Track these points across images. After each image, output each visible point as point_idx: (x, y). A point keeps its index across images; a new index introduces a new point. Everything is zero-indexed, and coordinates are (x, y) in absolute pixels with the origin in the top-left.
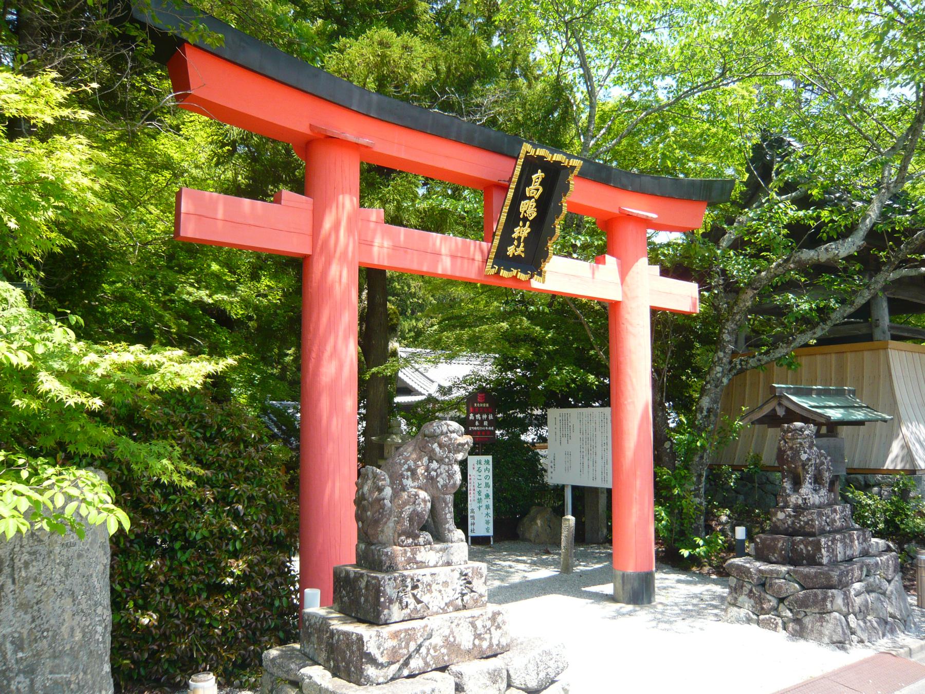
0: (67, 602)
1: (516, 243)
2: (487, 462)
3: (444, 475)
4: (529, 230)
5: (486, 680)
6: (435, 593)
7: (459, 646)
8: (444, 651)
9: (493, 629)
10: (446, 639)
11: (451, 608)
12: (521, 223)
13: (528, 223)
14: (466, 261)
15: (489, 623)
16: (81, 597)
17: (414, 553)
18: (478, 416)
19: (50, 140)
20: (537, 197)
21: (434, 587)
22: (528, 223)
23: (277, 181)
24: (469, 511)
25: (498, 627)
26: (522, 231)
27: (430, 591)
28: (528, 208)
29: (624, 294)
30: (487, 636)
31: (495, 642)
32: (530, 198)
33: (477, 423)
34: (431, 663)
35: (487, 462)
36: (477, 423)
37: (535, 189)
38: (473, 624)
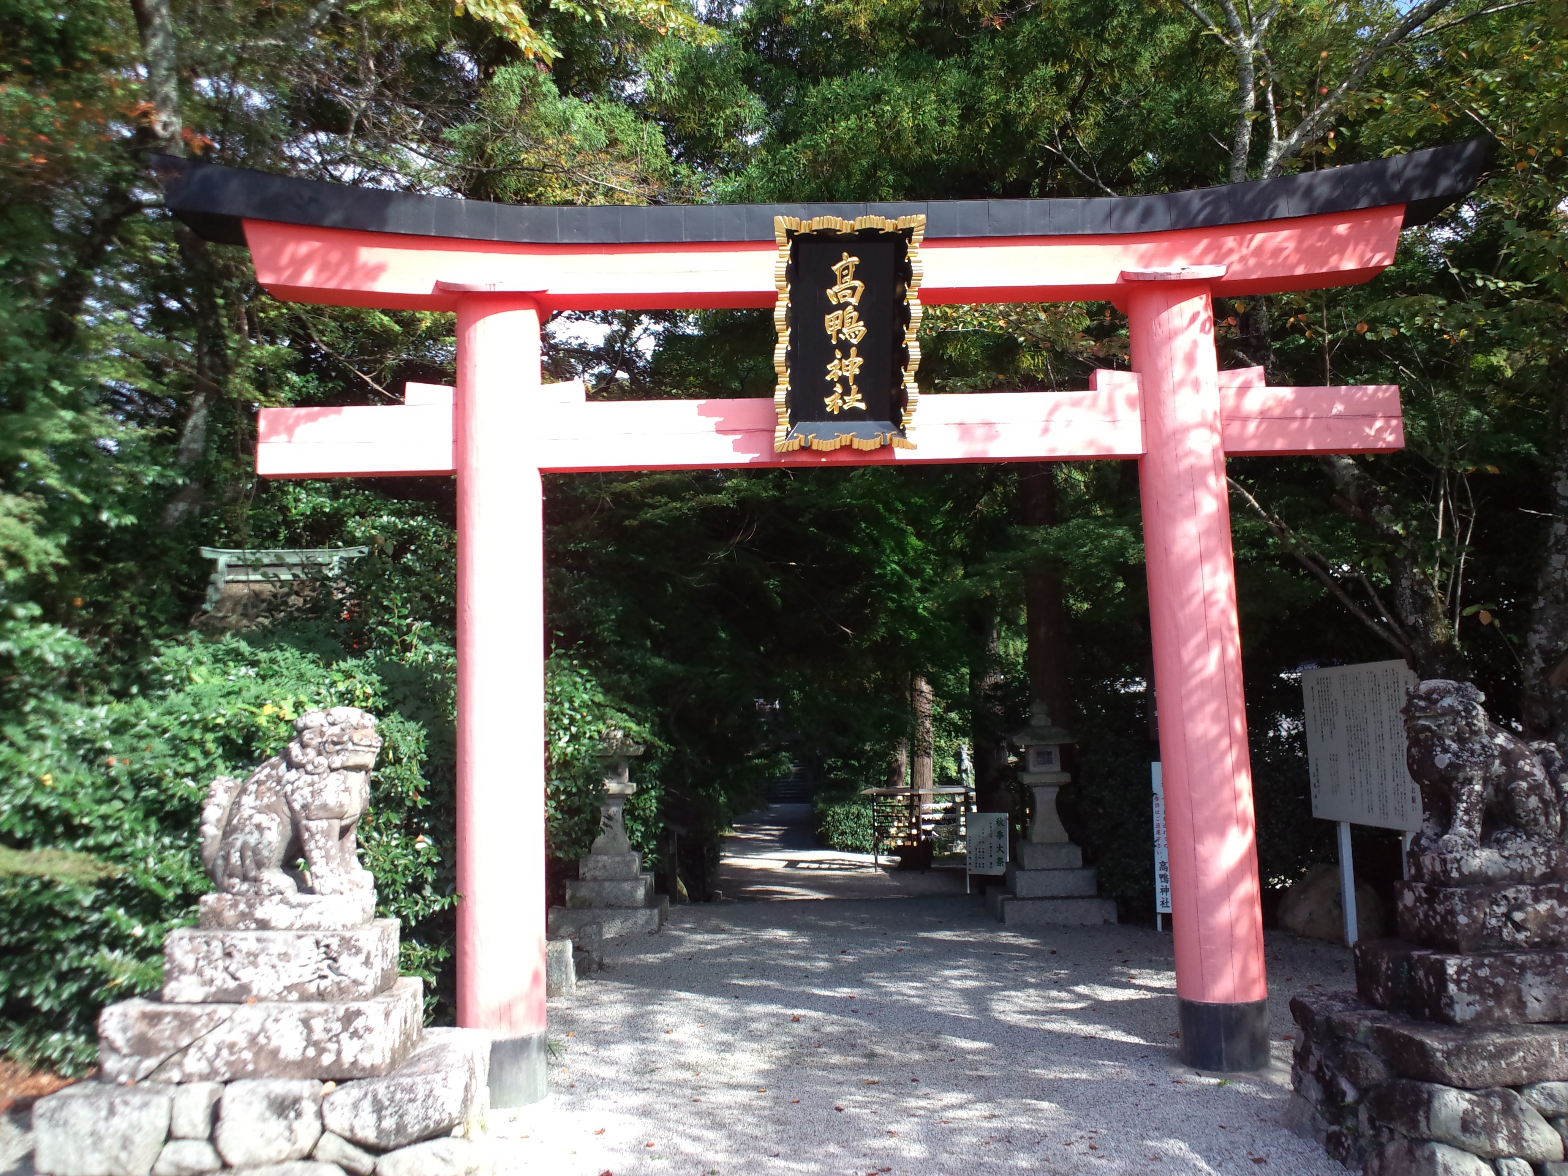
1: (838, 389)
3: (306, 792)
4: (859, 361)
5: (260, 1106)
6: (264, 969)
7: (275, 1052)
8: (247, 1055)
9: (345, 1037)
10: (253, 1040)
11: (295, 995)
12: (838, 354)
13: (853, 351)
15: (337, 1027)
17: (251, 906)
19: (1106, 340)
20: (854, 301)
21: (262, 959)
22: (853, 351)
24: (1157, 866)
25: (355, 1034)
26: (846, 367)
27: (255, 964)
28: (847, 325)
30: (333, 1046)
32: (843, 306)
34: (223, 1070)
37: (846, 290)
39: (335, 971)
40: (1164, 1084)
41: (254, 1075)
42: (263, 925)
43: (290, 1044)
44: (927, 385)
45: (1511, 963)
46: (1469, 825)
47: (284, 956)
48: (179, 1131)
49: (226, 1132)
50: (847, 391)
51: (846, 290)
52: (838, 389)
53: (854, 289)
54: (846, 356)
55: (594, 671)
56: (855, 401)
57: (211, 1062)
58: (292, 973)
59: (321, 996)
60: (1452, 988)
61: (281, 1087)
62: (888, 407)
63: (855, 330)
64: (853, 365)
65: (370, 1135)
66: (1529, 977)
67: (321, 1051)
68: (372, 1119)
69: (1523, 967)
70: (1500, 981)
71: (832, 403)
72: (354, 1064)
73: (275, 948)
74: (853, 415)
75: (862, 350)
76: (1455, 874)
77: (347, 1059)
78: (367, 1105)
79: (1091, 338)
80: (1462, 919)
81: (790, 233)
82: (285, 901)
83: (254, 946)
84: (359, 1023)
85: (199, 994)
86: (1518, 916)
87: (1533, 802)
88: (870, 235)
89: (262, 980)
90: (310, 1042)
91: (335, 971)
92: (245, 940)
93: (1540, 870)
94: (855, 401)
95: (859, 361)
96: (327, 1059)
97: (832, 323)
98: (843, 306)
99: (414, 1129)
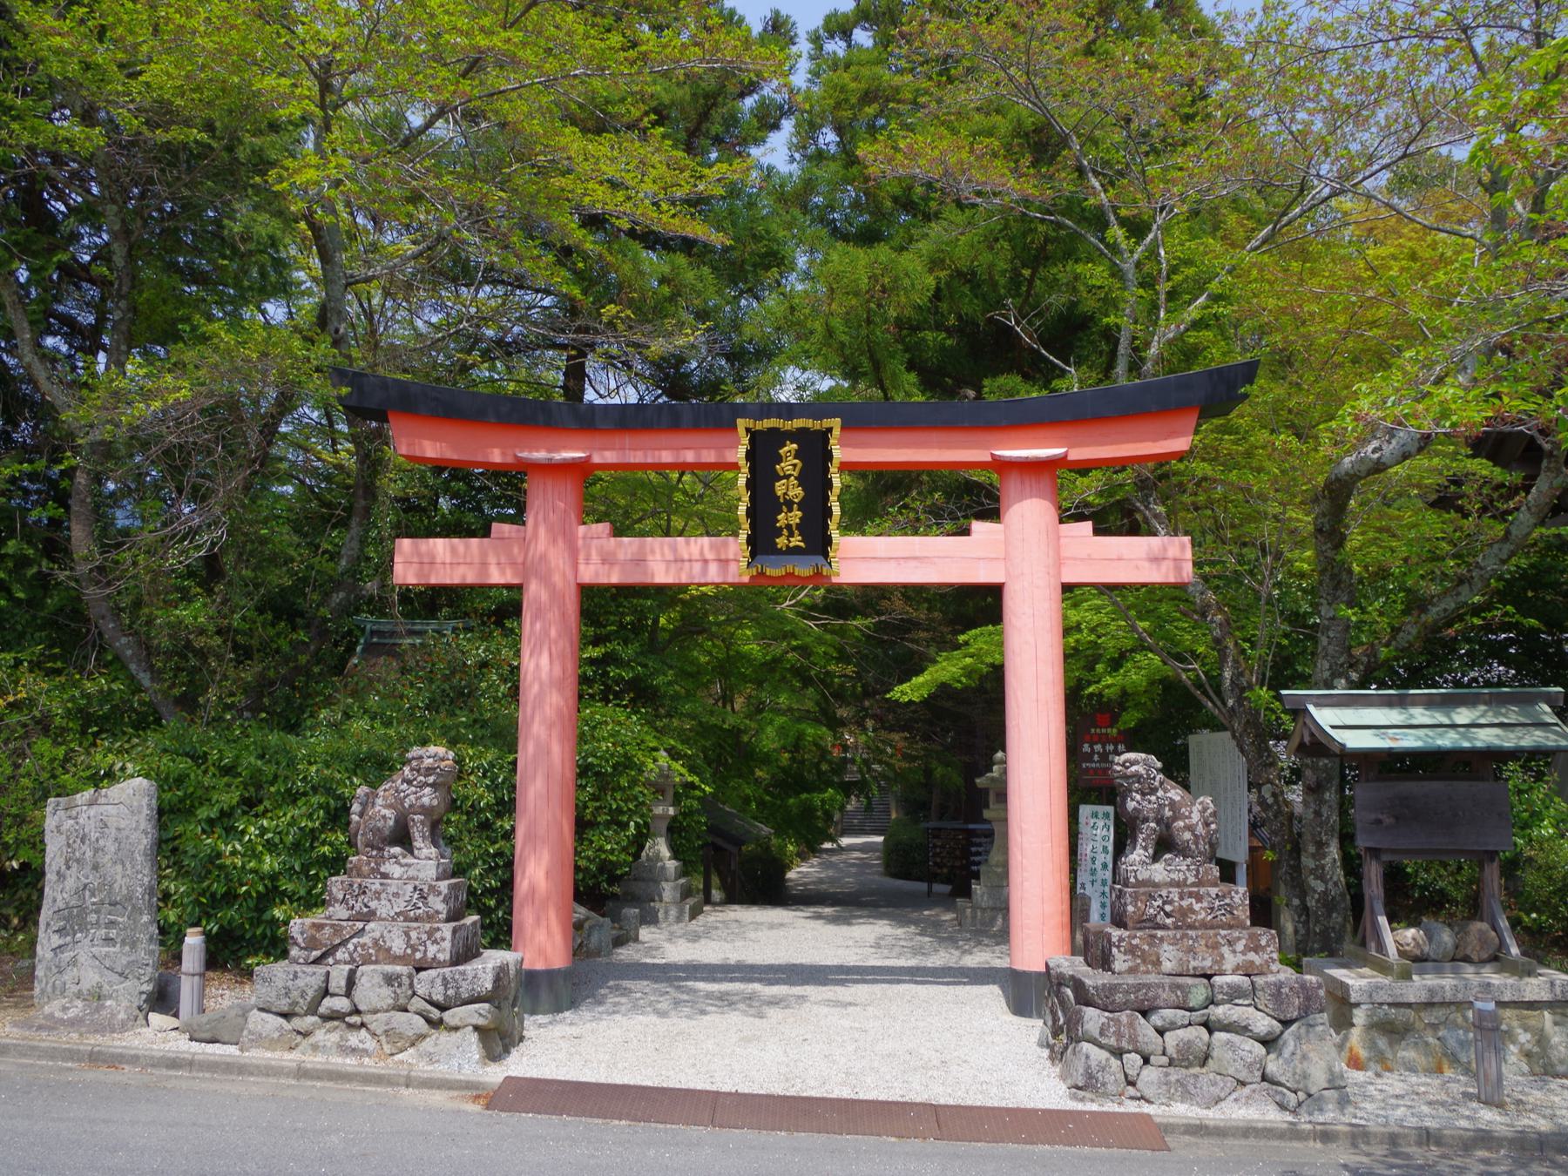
0: (119, 868)
1: (785, 532)
2: (1106, 815)
3: (412, 797)
5: (378, 979)
10: (376, 942)
14: (686, 557)
15: (424, 937)
16: (128, 865)
17: (378, 864)
18: (1098, 747)
21: (383, 896)
23: (1236, 387)
25: (435, 942)
27: (379, 899)
28: (789, 488)
29: (1008, 573)
31: (430, 955)
32: (787, 477)
33: (1096, 758)
35: (1106, 815)
36: (1096, 758)
37: (789, 462)
38: (407, 934)
39: (426, 905)
40: (890, 992)
41: (376, 962)
42: (385, 876)
43: (398, 945)
44: (846, 529)
45: (1154, 936)
46: (1145, 849)
47: (396, 895)
48: (331, 990)
49: (358, 994)
50: (791, 535)
51: (789, 462)
52: (785, 532)
53: (795, 466)
54: (790, 510)
55: (268, 955)
56: (796, 541)
57: (351, 955)
58: (400, 905)
59: (416, 919)
60: (1114, 950)
61: (389, 968)
62: (819, 544)
63: (797, 492)
64: (795, 517)
65: (438, 997)
66: (1165, 946)
67: (415, 950)
68: (441, 989)
69: (1162, 939)
70: (1146, 947)
71: (781, 542)
72: (434, 959)
73: (391, 890)
74: (796, 551)
75: (802, 506)
76: (1132, 880)
77: (430, 955)
78: (439, 981)
79: (969, 501)
80: (1130, 909)
81: (748, 430)
82: (397, 863)
83: (377, 886)
84: (438, 935)
85: (345, 914)
86: (1168, 908)
87: (1187, 836)
88: (803, 431)
89: (383, 908)
90: (408, 945)
91: (426, 905)
92: (375, 884)
93: (1191, 880)
94: (796, 541)
95: (799, 514)
96: (418, 955)
97: (780, 487)
98: (787, 477)
99: (465, 995)
